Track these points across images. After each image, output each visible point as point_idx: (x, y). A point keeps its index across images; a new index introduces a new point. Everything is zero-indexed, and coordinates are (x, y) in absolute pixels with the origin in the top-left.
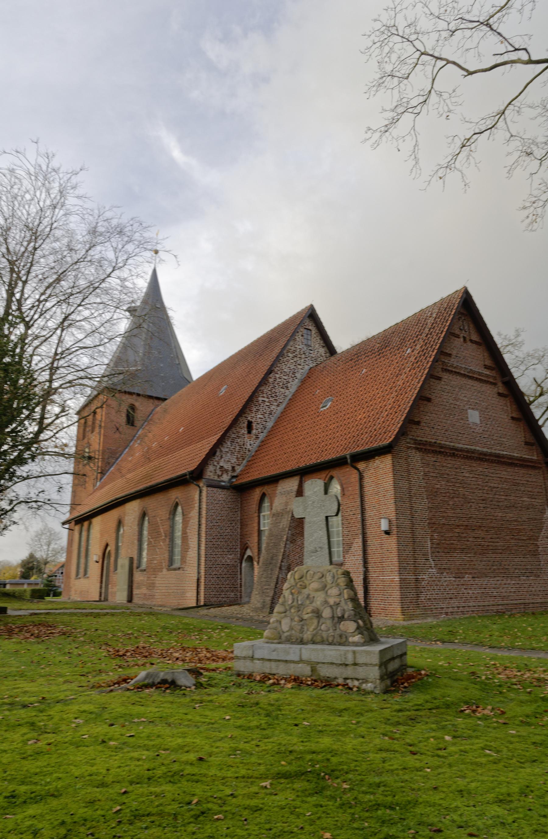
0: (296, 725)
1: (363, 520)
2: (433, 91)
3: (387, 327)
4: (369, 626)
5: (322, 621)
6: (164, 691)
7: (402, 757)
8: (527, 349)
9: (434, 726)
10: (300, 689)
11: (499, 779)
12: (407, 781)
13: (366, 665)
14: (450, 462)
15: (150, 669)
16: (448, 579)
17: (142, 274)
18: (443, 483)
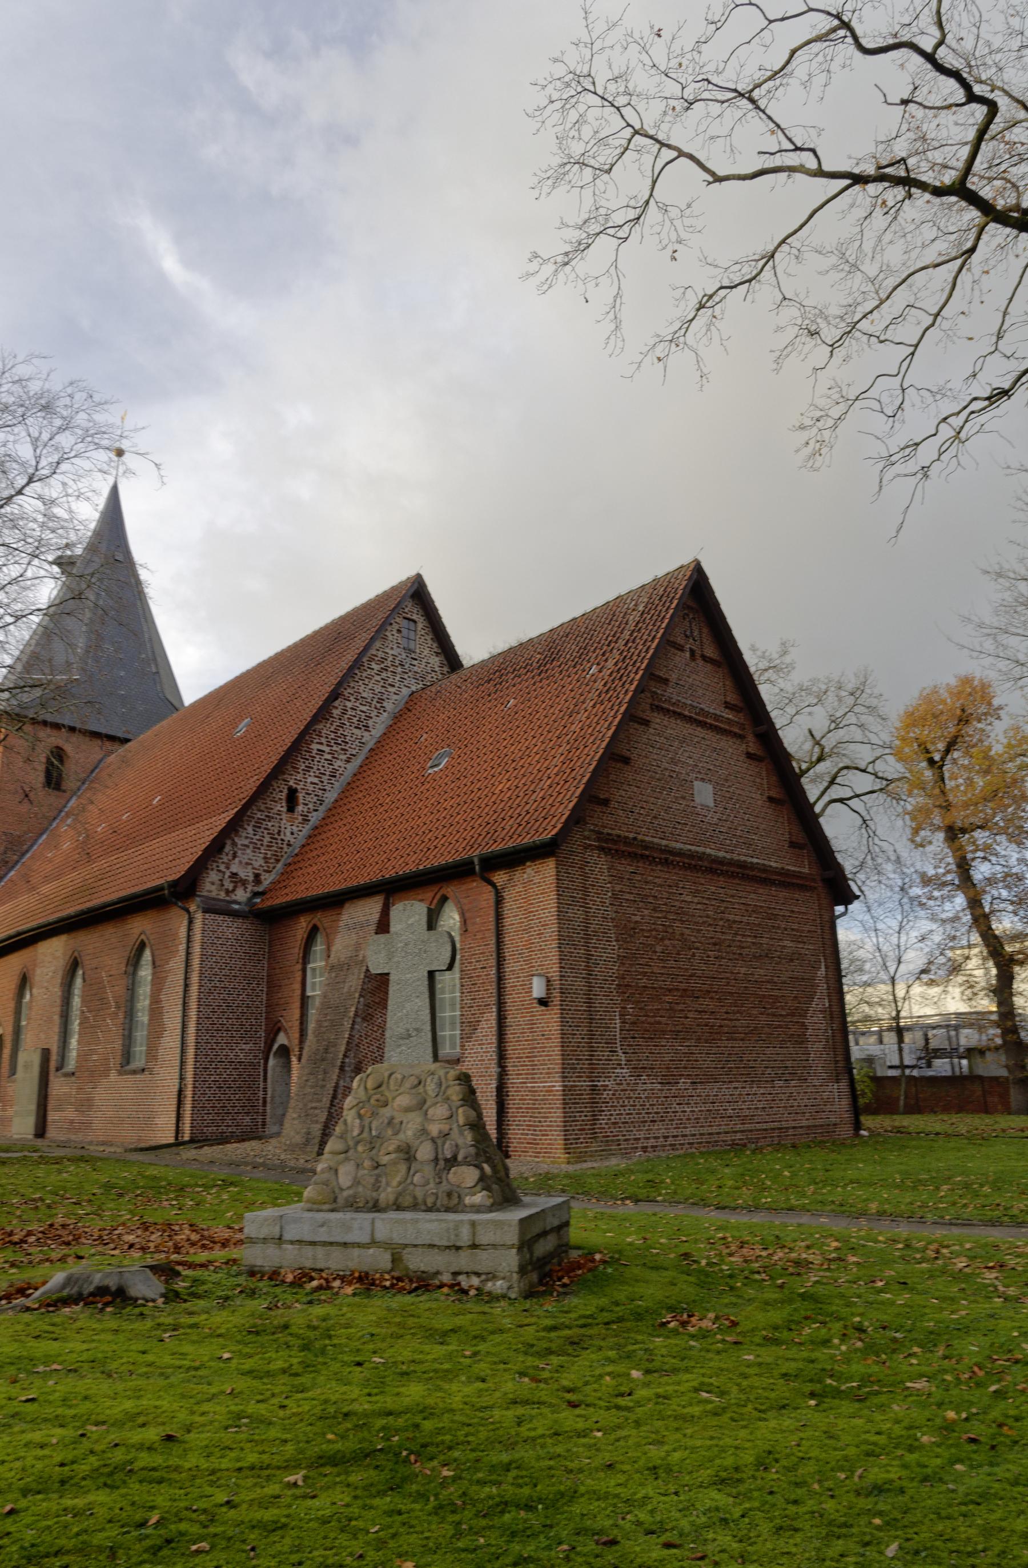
0: (359, 1364)
1: (500, 979)
4: (502, 1174)
6: (102, 1310)
8: (799, 676)
13: (494, 1246)
15: (74, 1268)
17: (90, 494)
18: (646, 912)
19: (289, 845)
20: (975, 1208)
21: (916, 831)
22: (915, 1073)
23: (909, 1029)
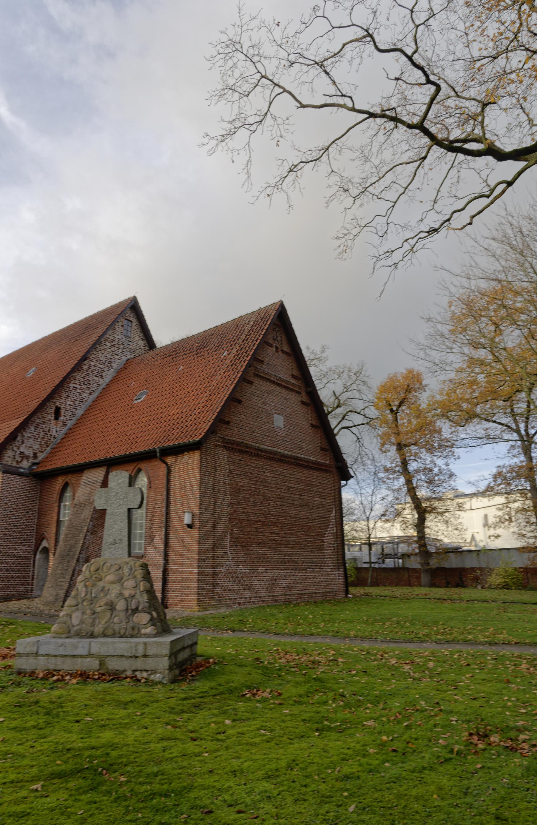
0: (78, 722)
1: (167, 513)
2: (269, 113)
3: (207, 328)
4: (163, 617)
5: (115, 613)
7: (183, 744)
8: (329, 364)
9: (216, 712)
10: (85, 684)
11: (270, 757)
12: (184, 767)
13: (156, 656)
14: (256, 462)
16: (243, 571)
18: (246, 481)
19: (54, 438)
20: (402, 634)
21: (383, 445)
22: (377, 566)
23: (375, 543)
